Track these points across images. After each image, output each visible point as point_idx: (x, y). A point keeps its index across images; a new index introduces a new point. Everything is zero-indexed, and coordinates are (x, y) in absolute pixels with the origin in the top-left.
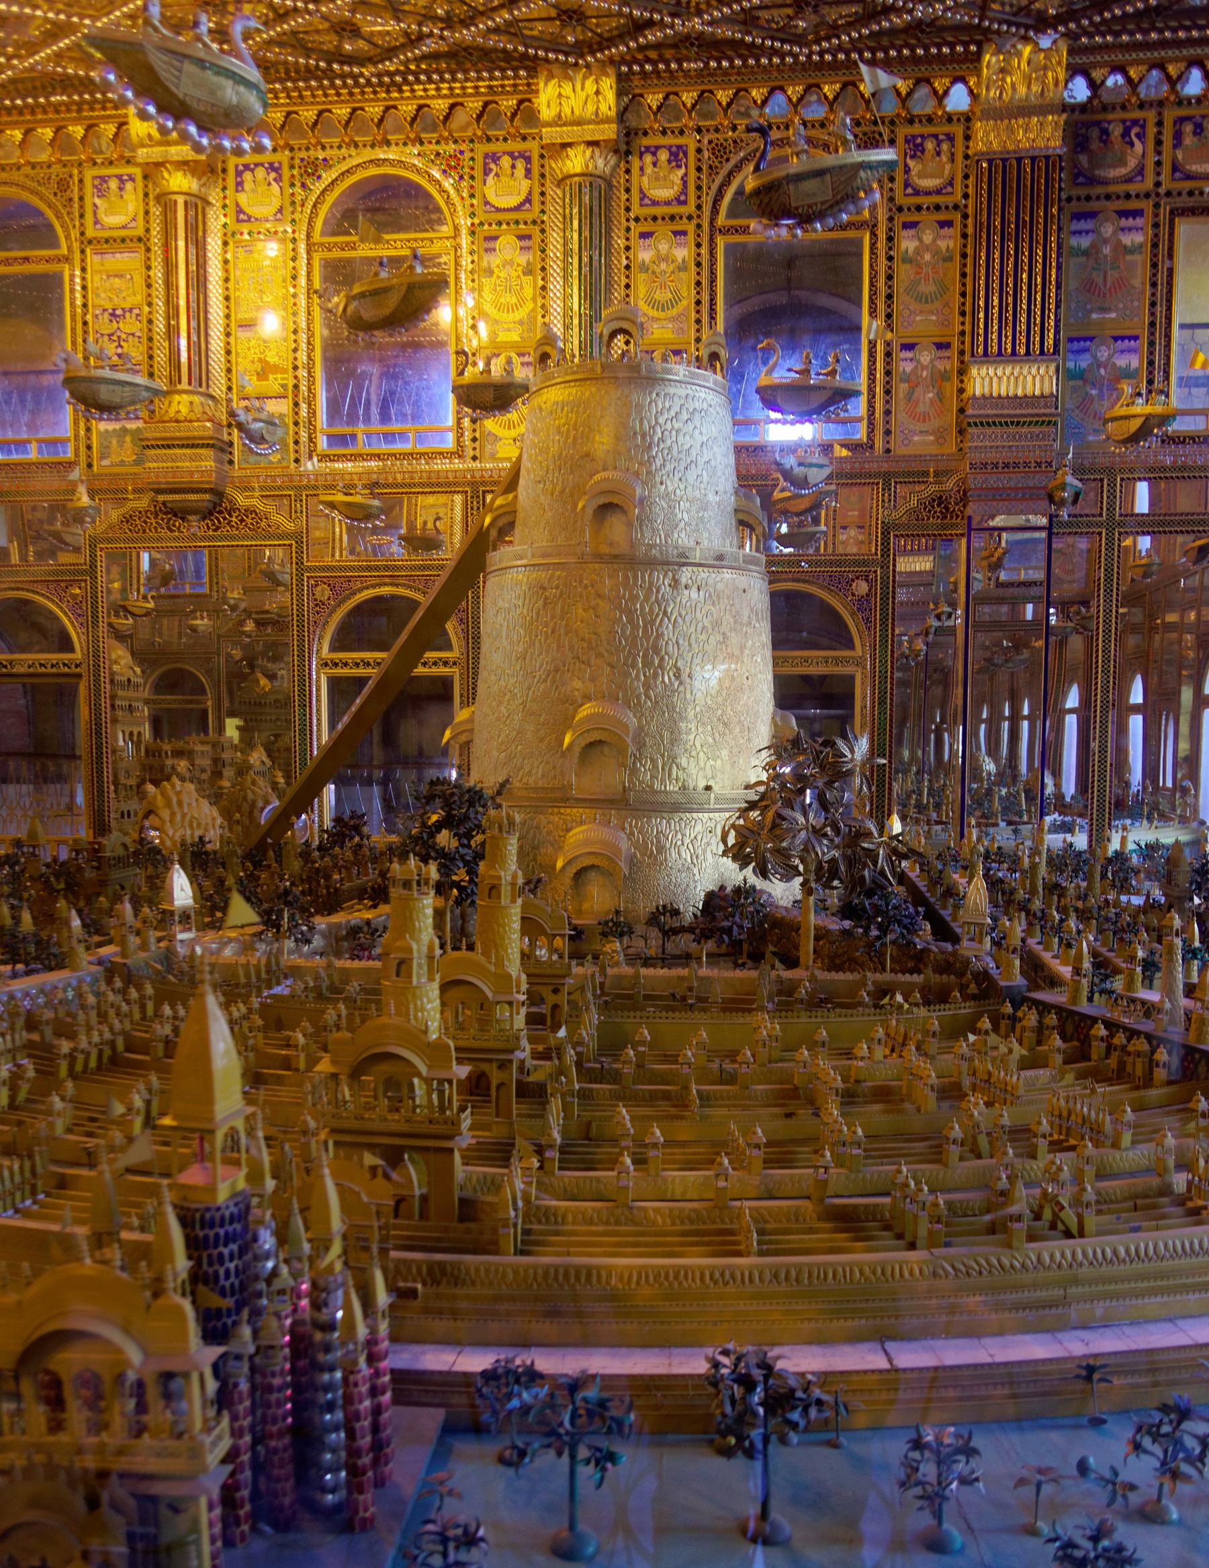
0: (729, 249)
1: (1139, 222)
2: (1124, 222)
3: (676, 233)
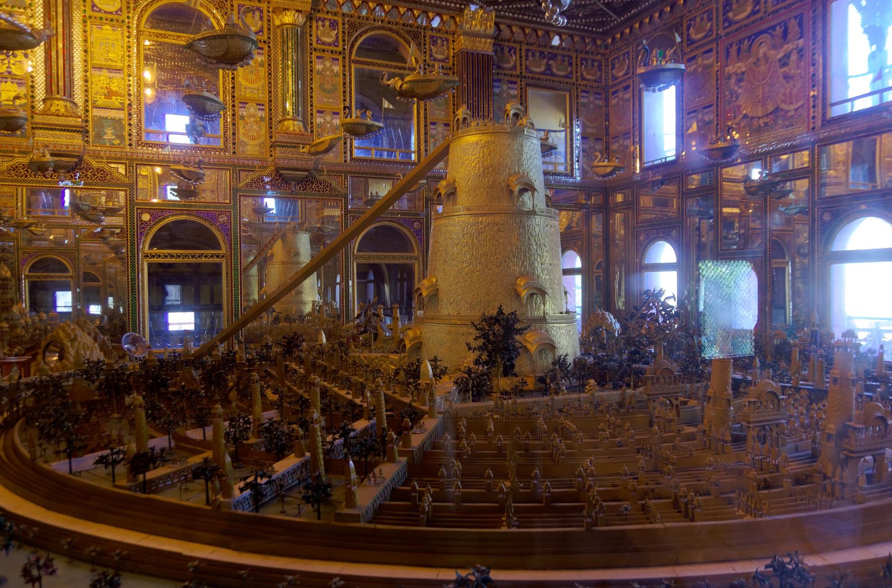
0: (357, 70)
1: (516, 86)
2: (510, 85)
3: (334, 59)
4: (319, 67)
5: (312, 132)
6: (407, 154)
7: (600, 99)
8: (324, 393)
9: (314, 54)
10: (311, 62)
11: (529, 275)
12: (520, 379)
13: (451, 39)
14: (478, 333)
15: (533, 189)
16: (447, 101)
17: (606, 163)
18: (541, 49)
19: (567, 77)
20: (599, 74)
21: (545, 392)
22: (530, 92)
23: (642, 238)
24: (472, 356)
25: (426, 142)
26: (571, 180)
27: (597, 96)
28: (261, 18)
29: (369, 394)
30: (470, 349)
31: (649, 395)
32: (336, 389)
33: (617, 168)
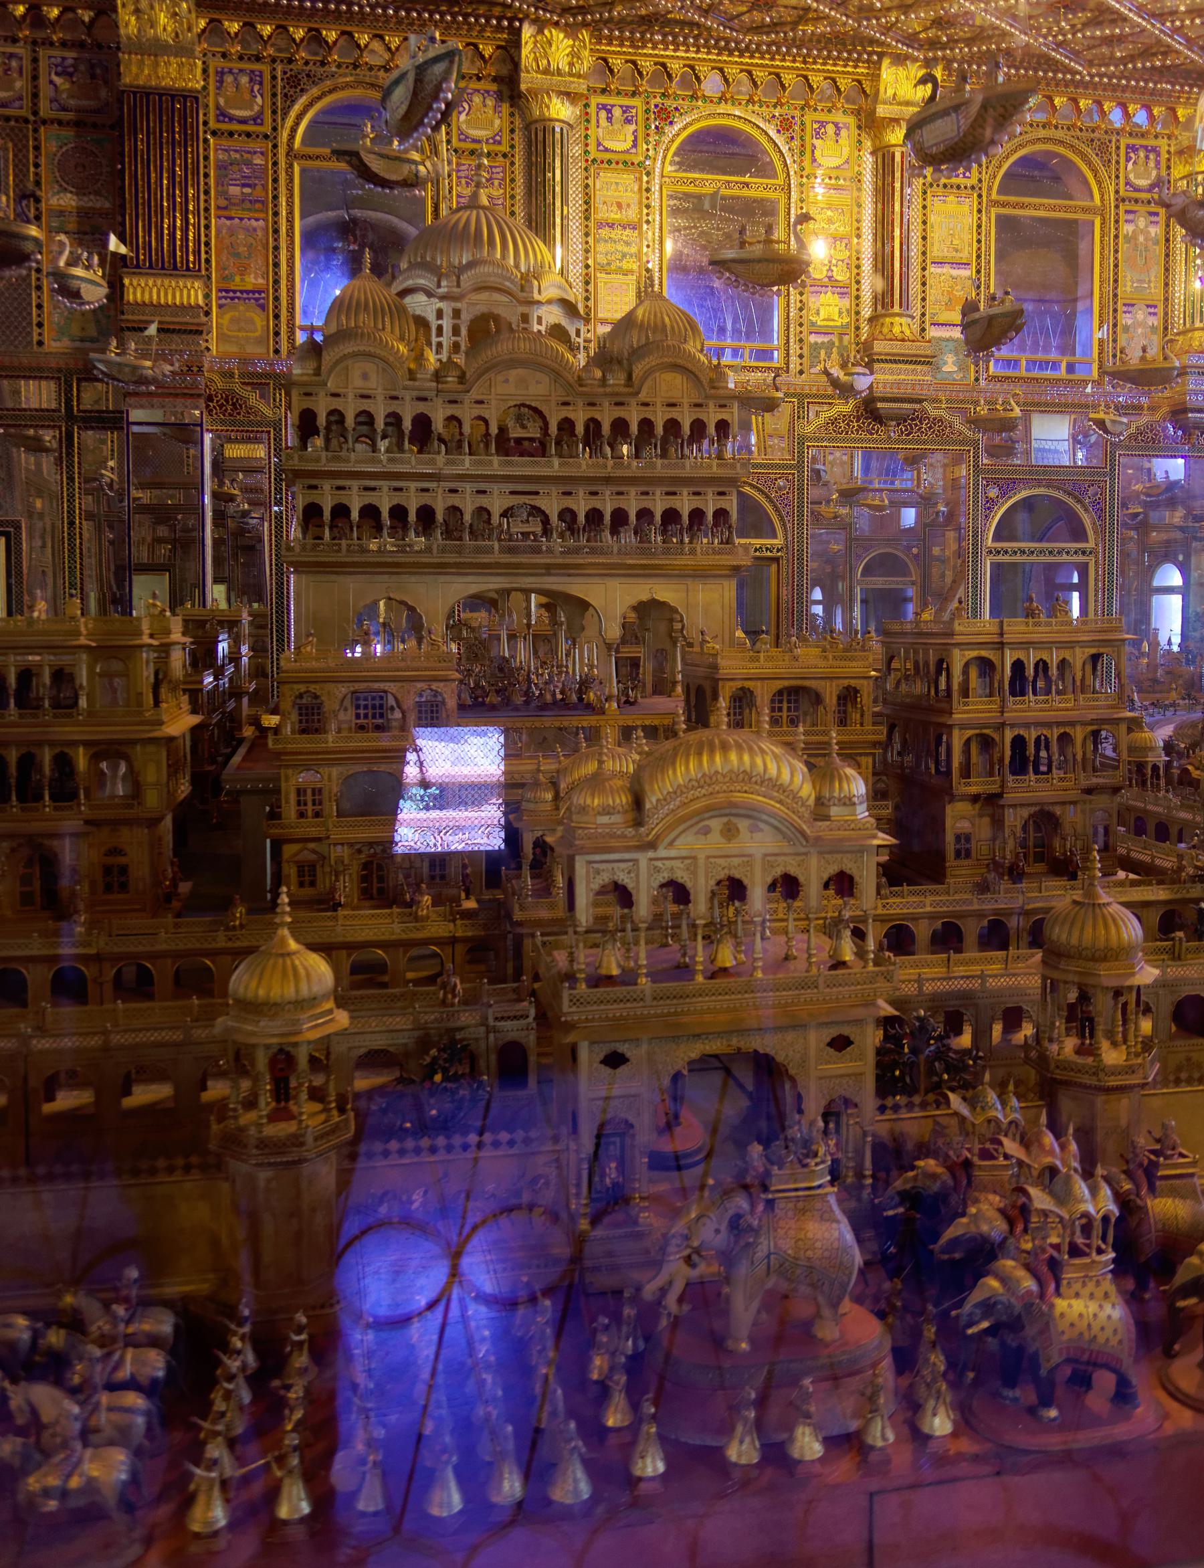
28: (1158, 163)
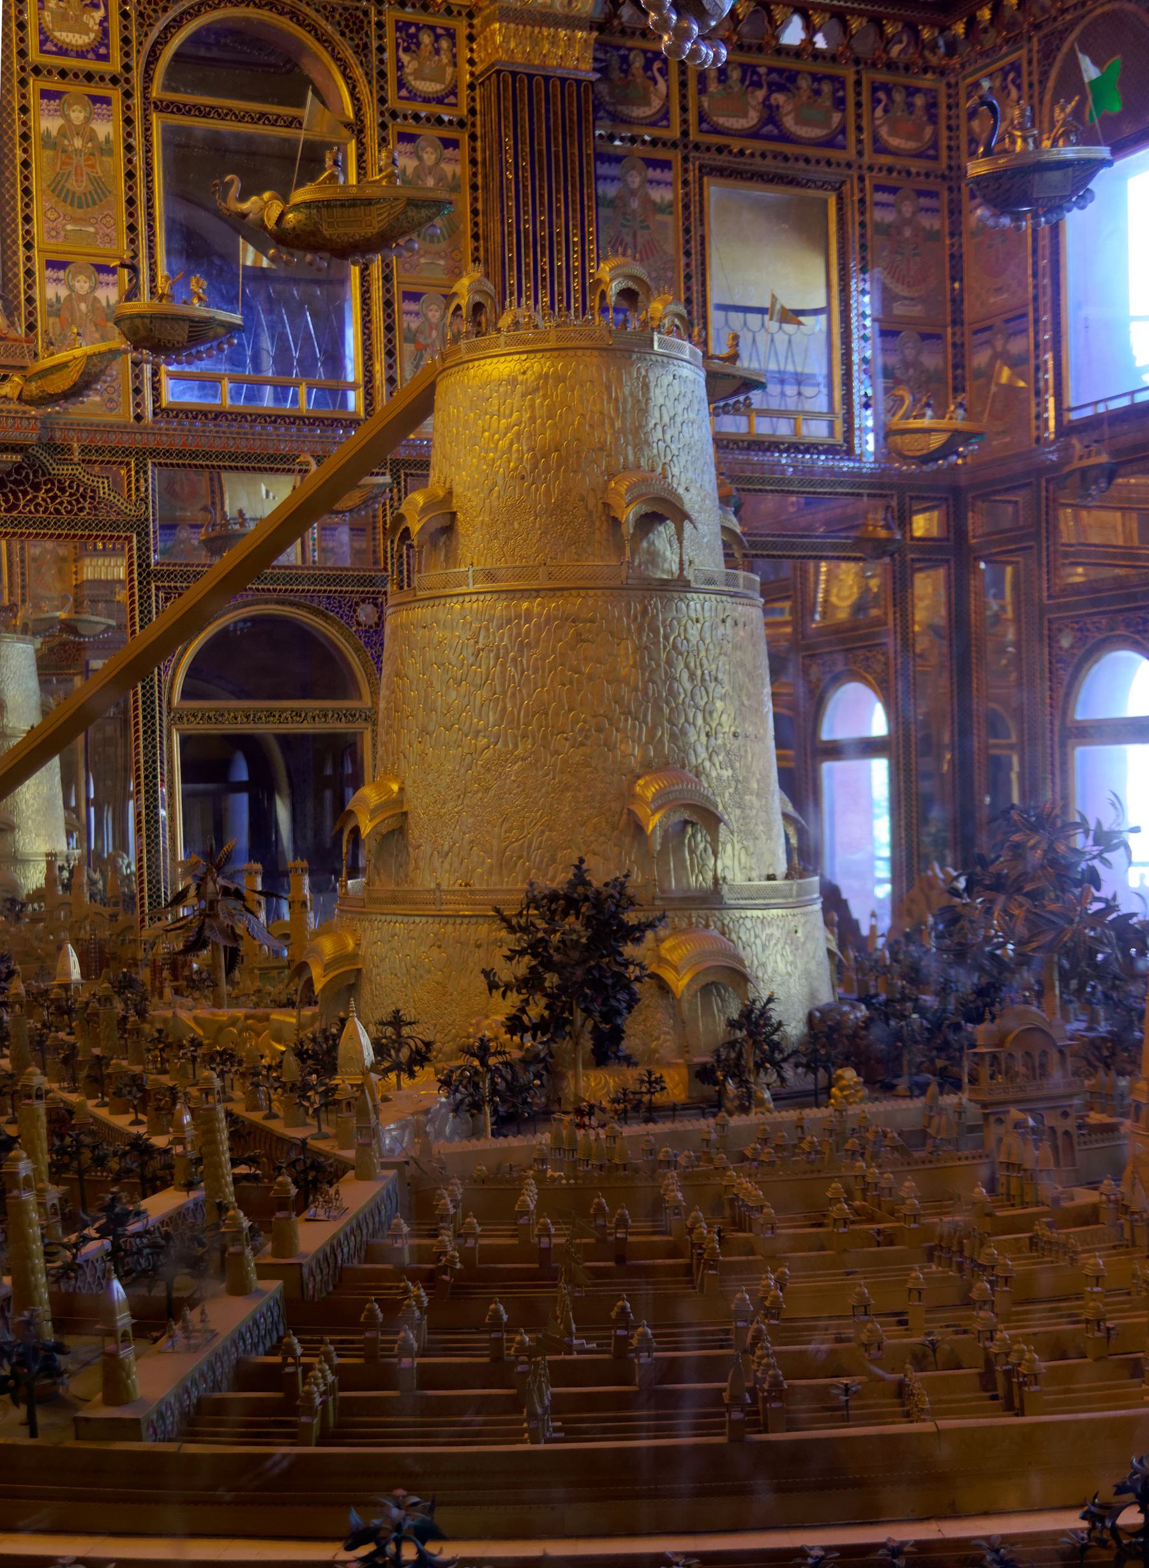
0: (166, 130)
1: (667, 176)
2: (652, 173)
3: (95, 99)
4: (48, 124)
5: (31, 327)
6: (334, 392)
7: (936, 211)
8: (61, 1120)
9: (34, 85)
10: (24, 110)
11: (672, 764)
12: (641, 1071)
13: (463, 31)
14: (511, 940)
15: (681, 516)
16: (453, 231)
17: (926, 422)
18: (746, 59)
19: (829, 143)
20: (928, 131)
21: (713, 1105)
22: (715, 191)
23: (1065, 642)
24: (504, 1006)
25: (390, 353)
26: (847, 465)
27: (924, 201)
29: (187, 1118)
30: (492, 986)
31: (984, 1106)
32: (103, 1113)
33: (957, 438)
